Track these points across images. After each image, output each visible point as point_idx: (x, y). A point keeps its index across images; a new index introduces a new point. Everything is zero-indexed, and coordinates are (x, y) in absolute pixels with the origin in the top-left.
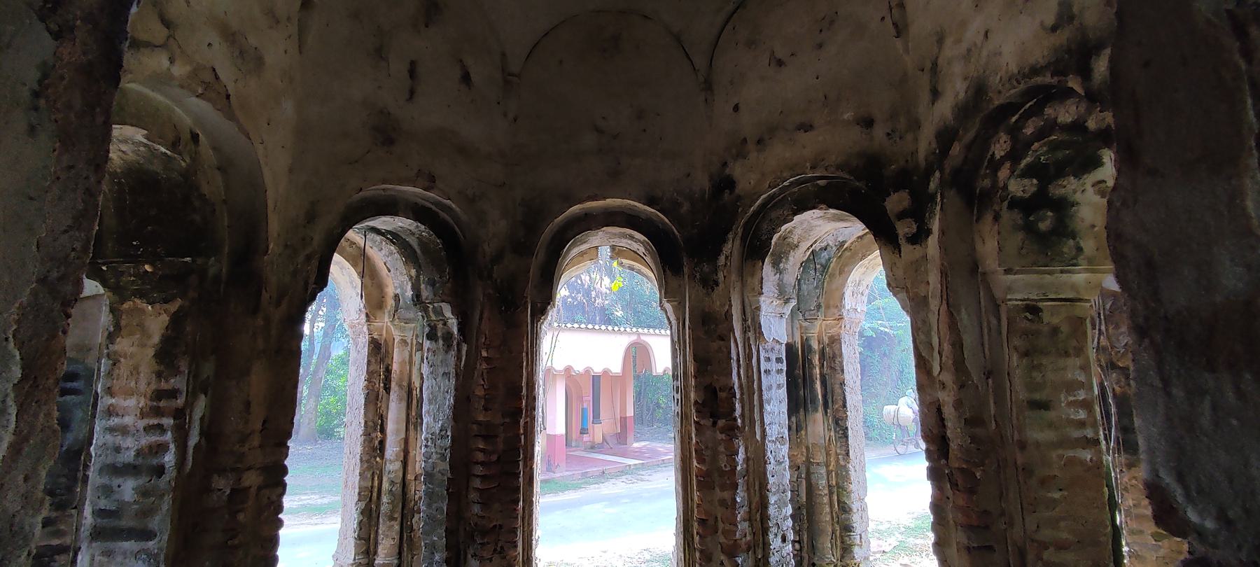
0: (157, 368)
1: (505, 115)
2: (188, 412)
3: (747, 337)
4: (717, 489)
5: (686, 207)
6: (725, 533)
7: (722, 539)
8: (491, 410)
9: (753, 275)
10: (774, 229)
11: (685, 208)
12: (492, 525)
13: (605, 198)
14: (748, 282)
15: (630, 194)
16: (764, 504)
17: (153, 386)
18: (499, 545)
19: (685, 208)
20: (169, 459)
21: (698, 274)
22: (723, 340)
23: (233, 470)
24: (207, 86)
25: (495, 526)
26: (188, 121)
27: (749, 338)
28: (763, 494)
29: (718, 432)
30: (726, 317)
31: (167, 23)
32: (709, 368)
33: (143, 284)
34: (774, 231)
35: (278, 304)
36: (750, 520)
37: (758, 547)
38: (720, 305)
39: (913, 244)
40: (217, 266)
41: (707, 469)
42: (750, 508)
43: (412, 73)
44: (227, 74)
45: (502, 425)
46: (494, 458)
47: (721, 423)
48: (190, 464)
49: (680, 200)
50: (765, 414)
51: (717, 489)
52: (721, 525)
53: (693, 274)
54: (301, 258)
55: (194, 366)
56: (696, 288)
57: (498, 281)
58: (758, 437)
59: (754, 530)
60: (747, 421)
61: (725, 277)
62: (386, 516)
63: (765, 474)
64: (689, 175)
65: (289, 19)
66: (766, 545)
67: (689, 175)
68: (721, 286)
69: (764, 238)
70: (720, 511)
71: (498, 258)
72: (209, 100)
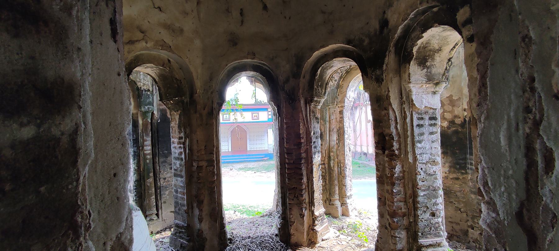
0: (178, 131)
1: (285, 18)
2: (185, 143)
3: (403, 107)
4: (386, 185)
5: (367, 41)
6: (389, 206)
7: (388, 209)
8: (288, 143)
9: (405, 72)
10: (413, 44)
11: (366, 42)
12: (293, 187)
13: (328, 46)
14: (403, 76)
15: (339, 41)
16: (415, 195)
17: (179, 136)
18: (296, 195)
19: (366, 42)
20: (183, 156)
21: (374, 76)
22: (386, 110)
23: (197, 160)
24: (162, 46)
25: (294, 187)
26: (166, 57)
27: (404, 108)
28: (415, 190)
29: (385, 157)
30: (387, 98)
31: (143, 32)
32: (381, 124)
33: (124, 116)
34: (413, 45)
35: (204, 110)
36: (405, 202)
37: (411, 216)
38: (384, 91)
39: (470, 43)
40: (186, 99)
41: (380, 175)
42: (406, 196)
43: (242, 14)
44: (168, 40)
45: (294, 149)
46: (292, 162)
47: (387, 152)
48: (187, 159)
49: (364, 38)
50: (416, 149)
51: (386, 185)
52: (387, 202)
53: (371, 76)
54: (209, 93)
55: (185, 130)
56: (373, 84)
57: (288, 91)
58: (411, 160)
59: (408, 207)
60: (403, 152)
61: (386, 76)
62: (469, 173)
63: (416, 180)
64: (368, 23)
65: (192, 11)
66: (416, 216)
67: (368, 23)
68: (385, 81)
69: (409, 50)
70: (387, 195)
71: (287, 81)
72: (164, 50)
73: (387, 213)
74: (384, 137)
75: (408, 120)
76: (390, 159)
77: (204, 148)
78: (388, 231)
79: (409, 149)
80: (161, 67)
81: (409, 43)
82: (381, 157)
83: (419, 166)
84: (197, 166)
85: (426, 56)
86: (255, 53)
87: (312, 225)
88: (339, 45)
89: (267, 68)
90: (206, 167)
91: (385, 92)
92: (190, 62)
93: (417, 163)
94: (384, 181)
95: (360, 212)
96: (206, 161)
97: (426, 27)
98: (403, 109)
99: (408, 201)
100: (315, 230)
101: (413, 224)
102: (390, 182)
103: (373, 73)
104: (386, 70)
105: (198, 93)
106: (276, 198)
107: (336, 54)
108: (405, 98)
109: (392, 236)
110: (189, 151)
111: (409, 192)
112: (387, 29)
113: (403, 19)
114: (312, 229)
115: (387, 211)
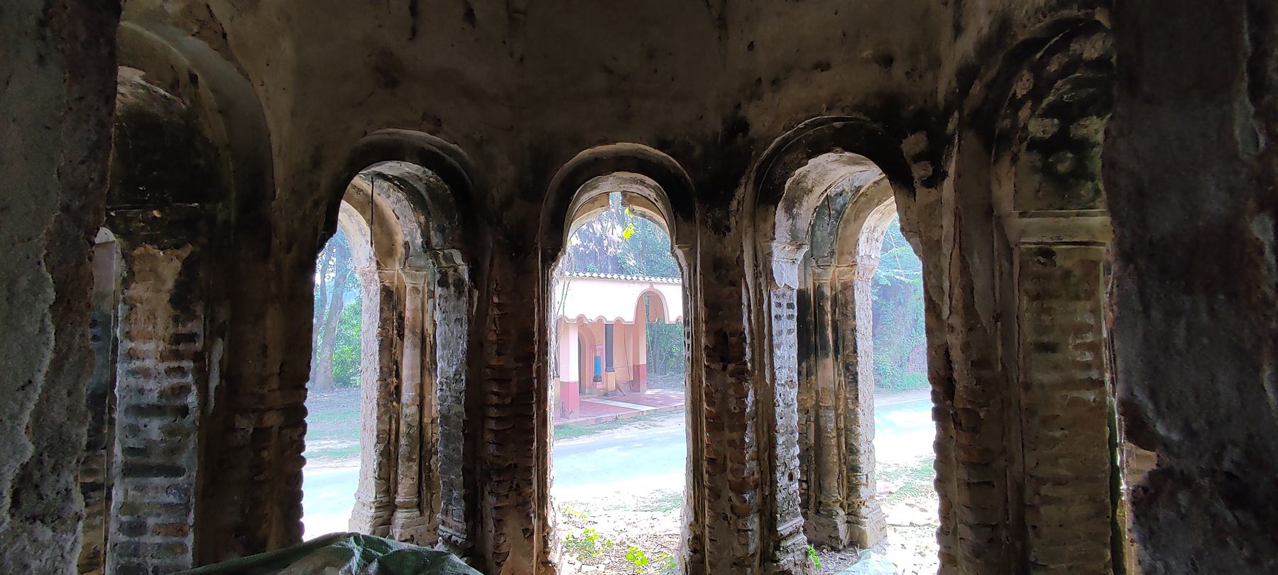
1: (511, 55)
3: (758, 283)
5: (698, 151)
7: (730, 477)
8: (503, 355)
9: (765, 220)
13: (615, 142)
16: (772, 444)
18: (515, 483)
20: (192, 400)
22: (734, 285)
24: (202, 24)
25: (511, 465)
35: (288, 251)
40: (226, 211)
41: (717, 412)
42: (758, 448)
46: (508, 401)
47: (731, 367)
56: (707, 234)
57: (508, 227)
61: (737, 222)
67: (701, 117)
72: (204, 39)
73: (728, 486)
74: (725, 337)
75: (765, 306)
76: (738, 379)
77: (279, 371)
78: (729, 523)
79: (767, 361)
80: (162, 92)
81: (779, 170)
82: (718, 376)
83: (779, 389)
84: (254, 429)
85: (795, 197)
86: (439, 120)
87: (542, 553)
88: (640, 146)
89: (457, 165)
90: (281, 428)
91: (734, 251)
92: (412, 109)
93: (776, 385)
94: (723, 423)
95: (567, 513)
96: (278, 410)
97: (817, 148)
98: (758, 286)
99: (762, 458)
100: (550, 562)
101: (768, 500)
102: (737, 423)
103: (709, 214)
104: (737, 211)
105: (277, 197)
106: (370, 514)
107: (425, 157)
108: (761, 266)
109: (739, 531)
110: (224, 382)
111: (765, 439)
112: (744, 136)
113: (786, 127)
114: (542, 563)
115: (728, 483)
